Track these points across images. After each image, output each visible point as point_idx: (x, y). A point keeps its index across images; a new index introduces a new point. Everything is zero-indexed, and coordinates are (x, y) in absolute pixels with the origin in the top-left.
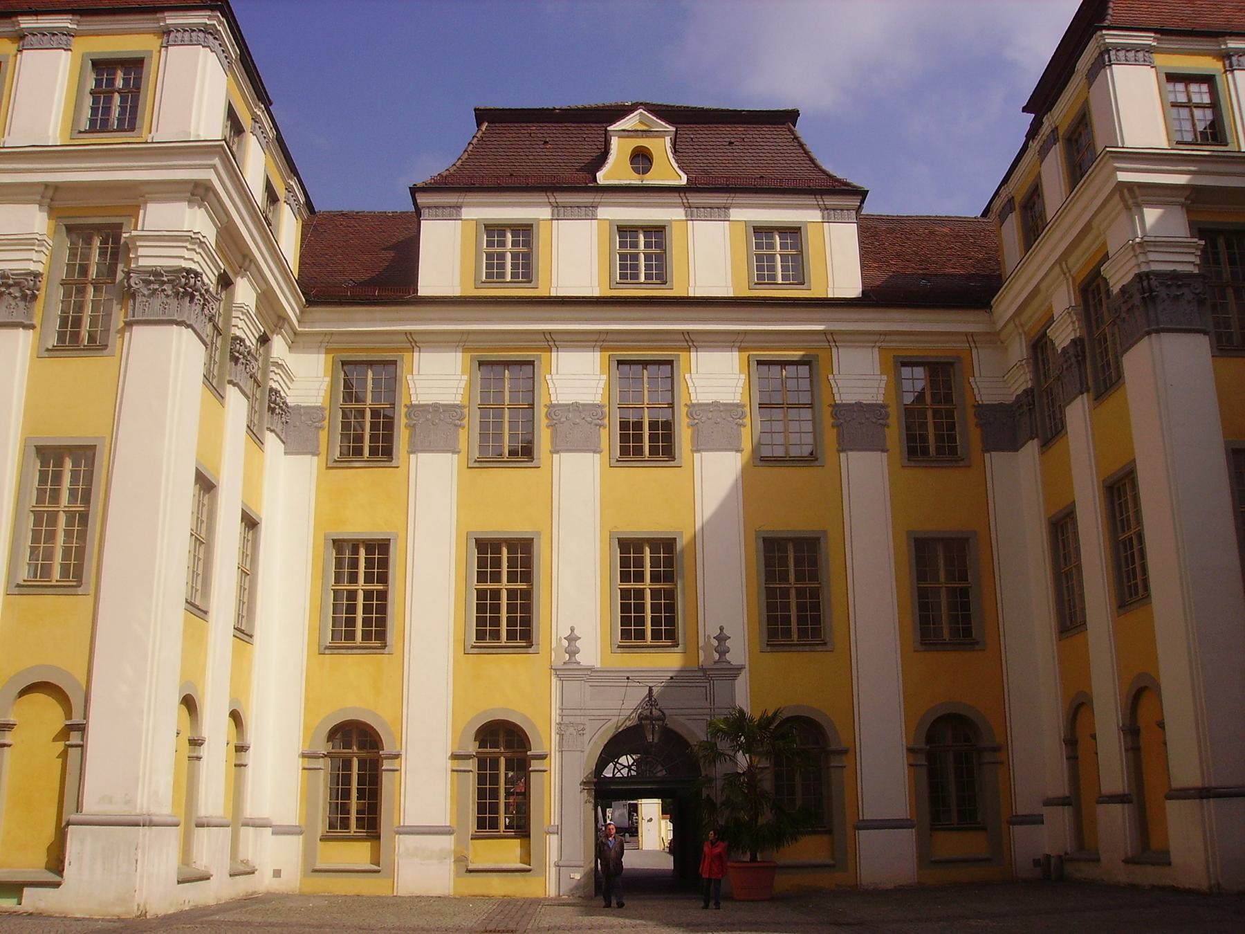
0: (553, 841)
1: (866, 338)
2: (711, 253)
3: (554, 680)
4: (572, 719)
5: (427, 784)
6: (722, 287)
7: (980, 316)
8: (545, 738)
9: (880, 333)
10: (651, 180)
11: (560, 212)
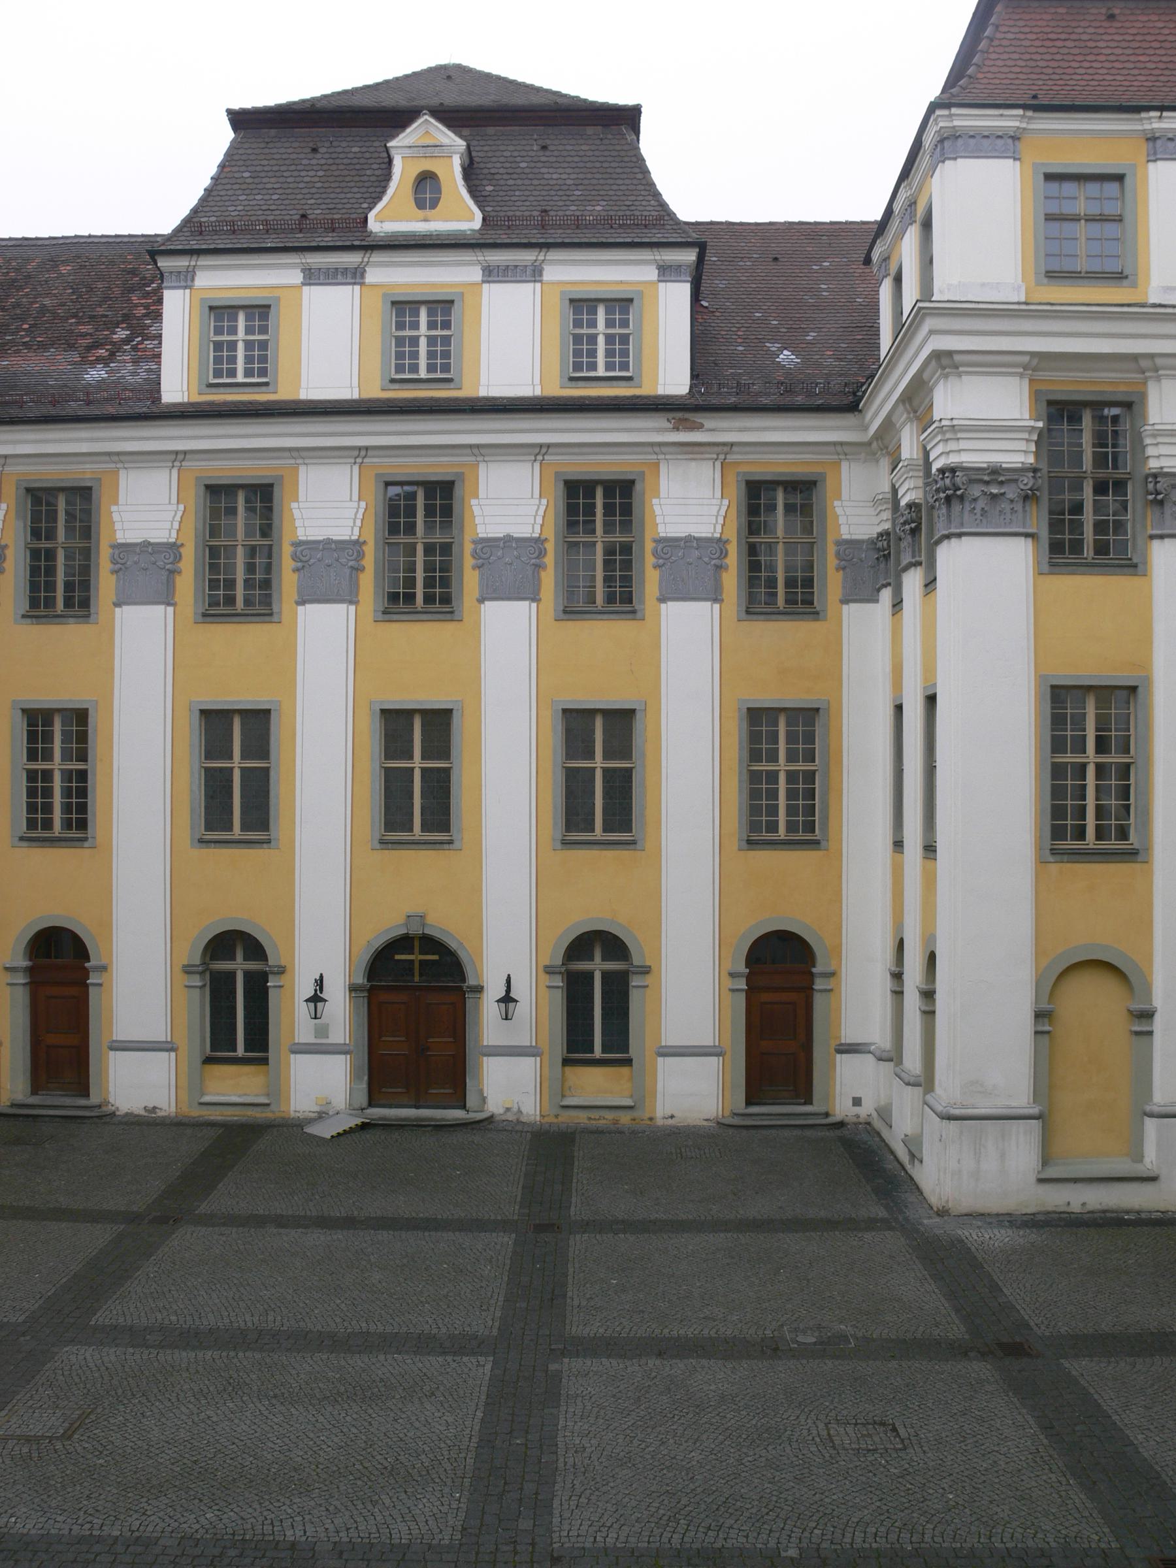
1: (346, 453)
2: (511, 337)
6: (344, 389)
7: (850, 419)
9: (835, 444)
11: (492, 274)
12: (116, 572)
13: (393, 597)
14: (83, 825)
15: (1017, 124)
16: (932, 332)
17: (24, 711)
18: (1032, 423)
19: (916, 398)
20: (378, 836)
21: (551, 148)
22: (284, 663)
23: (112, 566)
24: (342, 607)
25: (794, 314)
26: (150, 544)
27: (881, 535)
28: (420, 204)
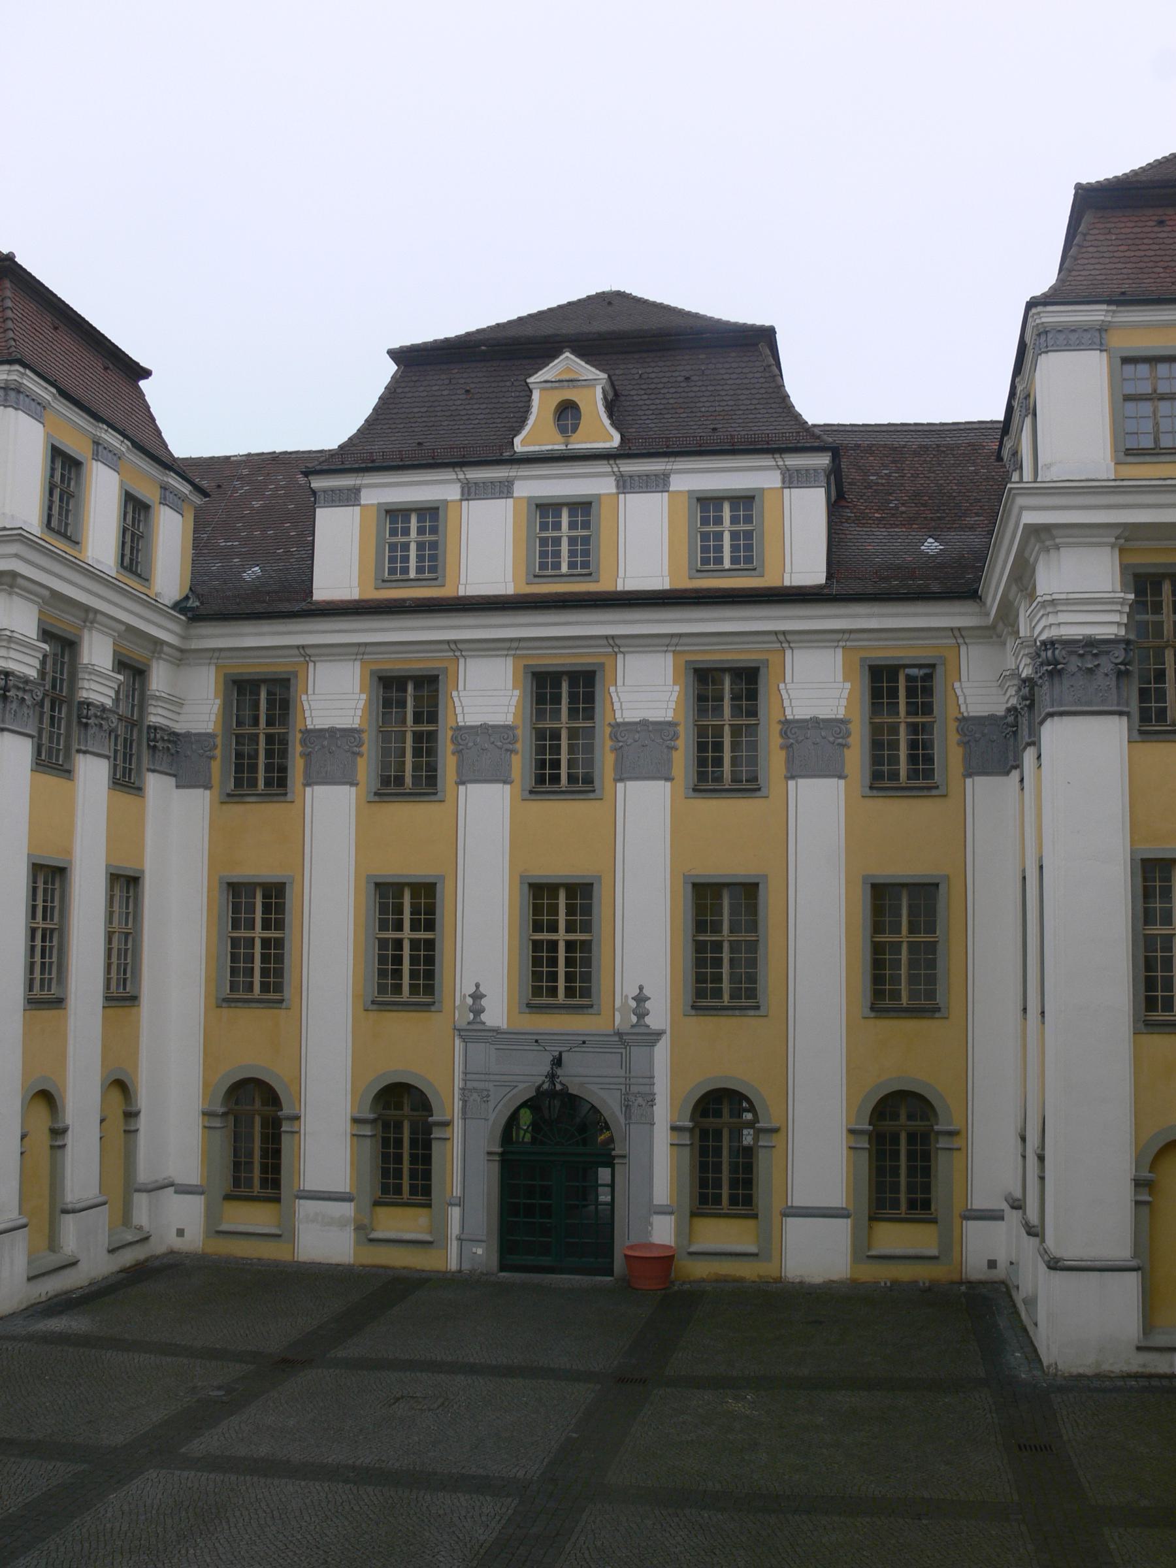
0: (455, 1213)
3: (457, 1041)
4: (475, 1084)
5: (327, 1148)
8: (449, 1103)
10: (579, 444)
11: (626, 484)
13: (385, 781)
14: (430, 990)
15: (1102, 318)
16: (16, 556)
17: (530, 885)
18: (1122, 595)
19: (1023, 575)
20: (869, 1004)
21: (707, 372)
22: (608, 837)
25: (923, 504)
27: (1009, 710)
28: (563, 430)
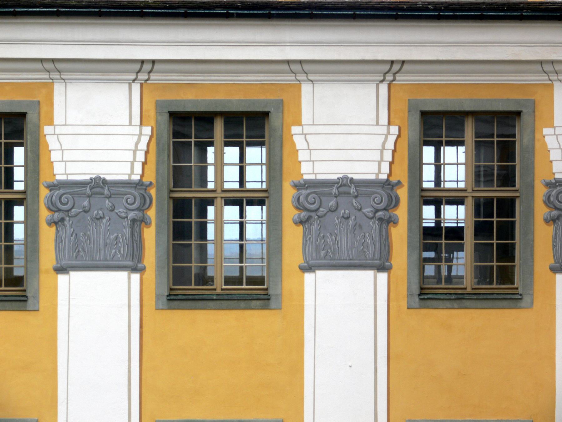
12: (301, 222)
23: (296, 212)
24: (122, 275)
26: (105, 182)
